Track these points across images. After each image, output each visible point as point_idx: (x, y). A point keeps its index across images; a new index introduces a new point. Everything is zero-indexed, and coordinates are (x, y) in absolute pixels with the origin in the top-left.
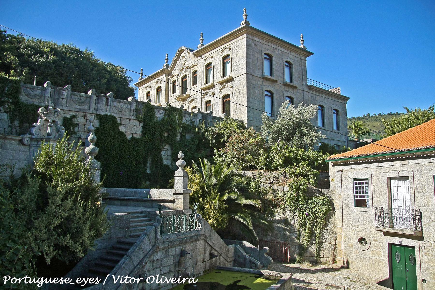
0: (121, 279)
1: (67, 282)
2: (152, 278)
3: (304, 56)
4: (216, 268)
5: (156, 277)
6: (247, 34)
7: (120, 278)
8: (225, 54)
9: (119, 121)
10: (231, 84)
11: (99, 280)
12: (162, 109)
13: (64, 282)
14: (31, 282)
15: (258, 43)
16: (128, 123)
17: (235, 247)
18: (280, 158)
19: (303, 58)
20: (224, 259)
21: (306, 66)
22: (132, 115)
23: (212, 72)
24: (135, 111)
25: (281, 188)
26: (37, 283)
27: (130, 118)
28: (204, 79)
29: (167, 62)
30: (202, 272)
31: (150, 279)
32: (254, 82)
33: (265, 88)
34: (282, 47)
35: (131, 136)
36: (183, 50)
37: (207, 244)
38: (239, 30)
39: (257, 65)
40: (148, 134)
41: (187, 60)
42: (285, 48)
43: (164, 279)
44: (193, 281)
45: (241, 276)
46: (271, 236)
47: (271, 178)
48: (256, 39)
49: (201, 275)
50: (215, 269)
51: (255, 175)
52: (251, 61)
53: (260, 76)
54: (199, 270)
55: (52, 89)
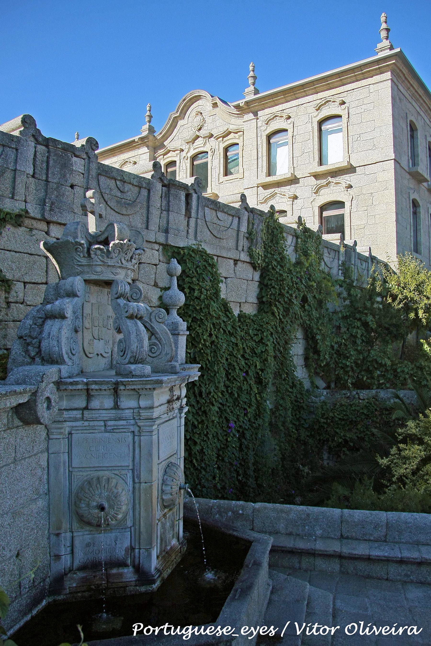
0: (308, 629)
1: (227, 632)
2: (353, 627)
5: (359, 626)
7: (306, 626)
8: (325, 112)
10: (347, 177)
11: (274, 629)
13: (223, 632)
14: (174, 632)
22: (240, 248)
26: (183, 635)
31: (350, 628)
43: (371, 629)
44: (415, 630)
55: (39, 147)
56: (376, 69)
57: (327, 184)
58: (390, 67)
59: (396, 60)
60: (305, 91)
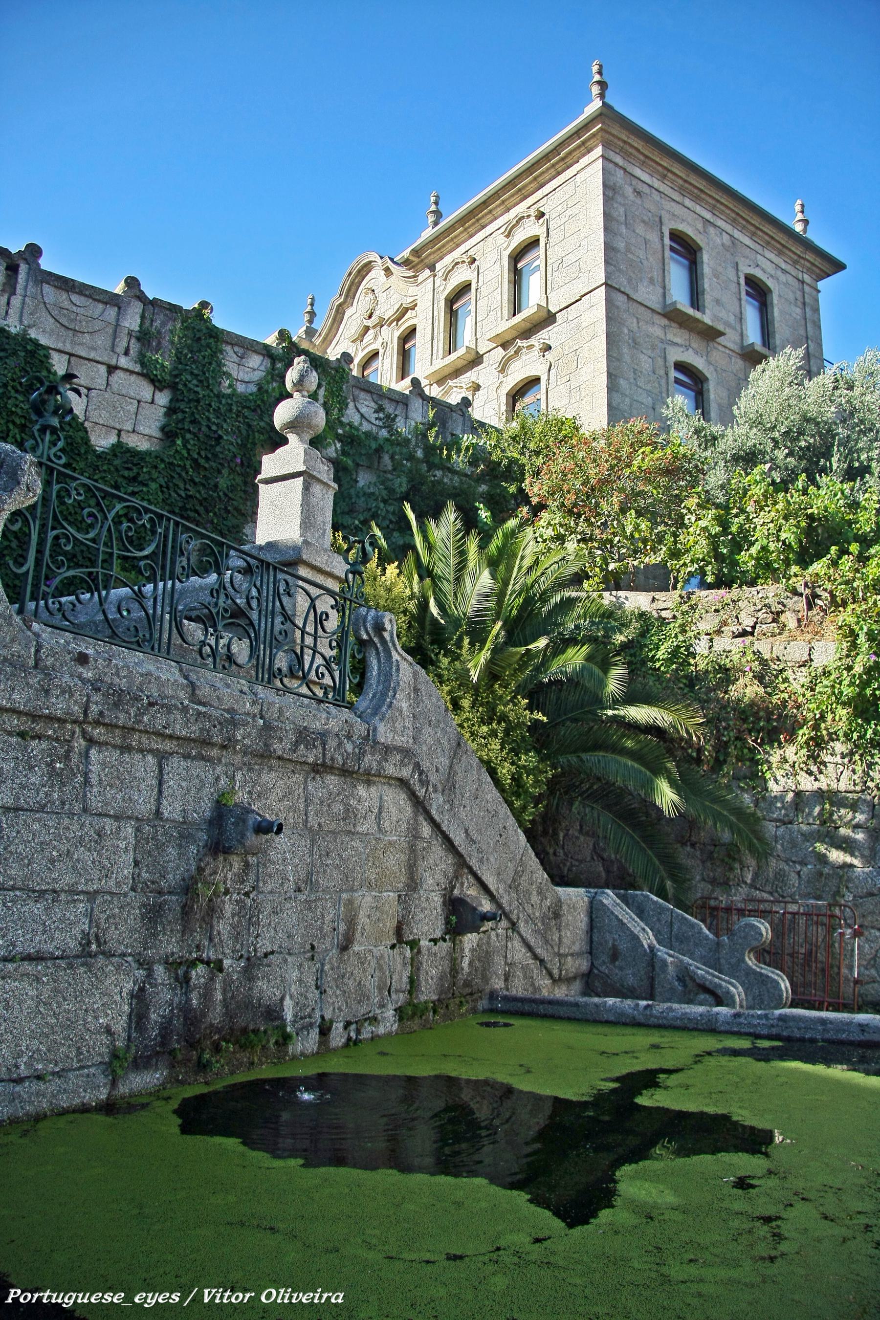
3: (810, 271)
4: (483, 1004)
6: (606, 145)
8: (521, 236)
9: (59, 365)
10: (544, 335)
12: (256, 352)
15: (646, 189)
16: (101, 382)
17: (591, 903)
18: (786, 518)
19: (807, 278)
20: (535, 957)
21: (816, 310)
22: (120, 349)
23: (469, 321)
24: (138, 339)
25: (797, 651)
27: (113, 362)
28: (441, 345)
29: (311, 321)
30: (390, 1013)
32: (635, 324)
33: (675, 355)
34: (734, 222)
35: (113, 439)
36: (367, 267)
37: (426, 830)
38: (577, 133)
39: (645, 262)
40: (188, 436)
41: (382, 297)
42: (744, 227)
45: (655, 1047)
46: (753, 886)
47: (742, 616)
48: (638, 172)
49: (381, 1030)
50: (474, 1011)
51: (663, 606)
52: (621, 245)
53: (657, 307)
54: (363, 997)
56: (579, 147)
57: (516, 352)
58: (599, 137)
59: (603, 123)
60: (490, 212)
